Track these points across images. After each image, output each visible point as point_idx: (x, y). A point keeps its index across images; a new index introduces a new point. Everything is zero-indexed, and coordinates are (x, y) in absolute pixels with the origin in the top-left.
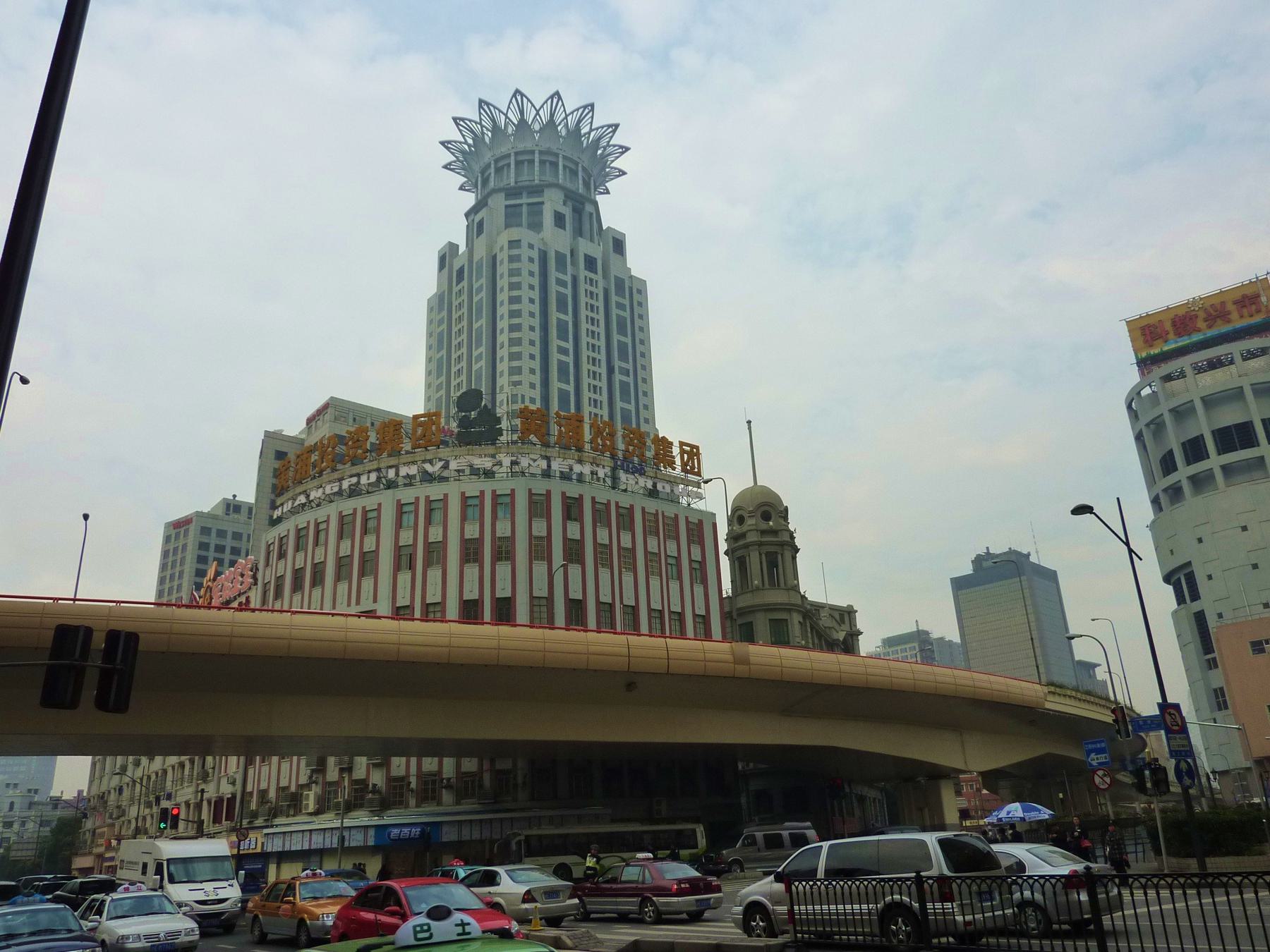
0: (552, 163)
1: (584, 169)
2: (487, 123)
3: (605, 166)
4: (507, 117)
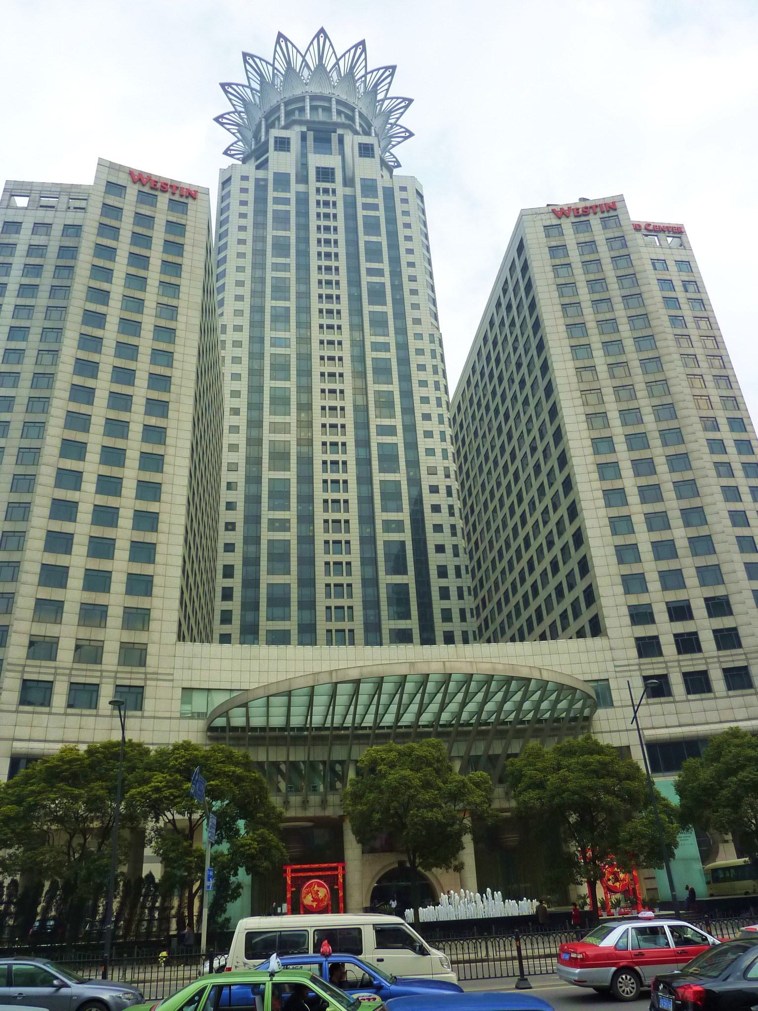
1: (361, 115)
2: (281, 66)
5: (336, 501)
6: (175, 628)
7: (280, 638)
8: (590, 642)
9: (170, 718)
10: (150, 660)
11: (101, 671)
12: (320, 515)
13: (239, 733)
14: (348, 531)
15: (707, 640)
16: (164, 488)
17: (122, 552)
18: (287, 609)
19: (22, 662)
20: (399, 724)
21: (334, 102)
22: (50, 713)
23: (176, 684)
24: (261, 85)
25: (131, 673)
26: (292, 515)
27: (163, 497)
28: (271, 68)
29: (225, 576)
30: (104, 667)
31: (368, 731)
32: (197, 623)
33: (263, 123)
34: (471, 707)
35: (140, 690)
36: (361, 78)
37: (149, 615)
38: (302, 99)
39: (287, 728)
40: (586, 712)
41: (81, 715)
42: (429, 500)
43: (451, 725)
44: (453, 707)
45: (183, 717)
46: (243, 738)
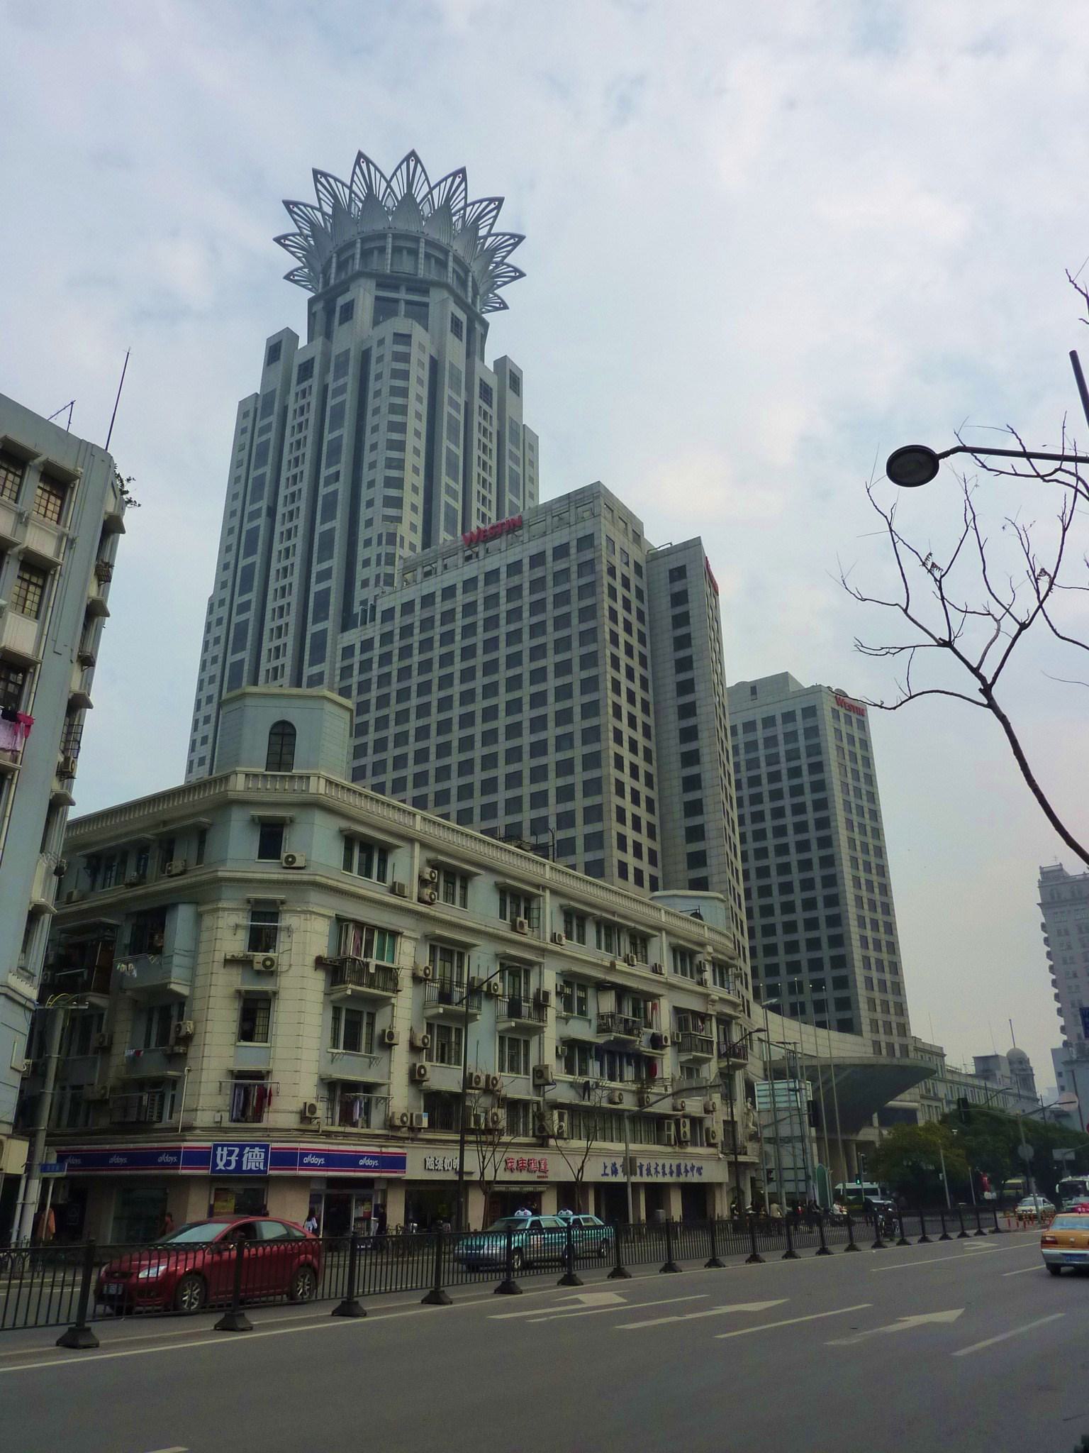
0: (438, 261)
2: (399, 188)
3: (493, 287)
4: (389, 186)
21: (422, 245)
24: (334, 208)
28: (347, 191)
33: (334, 260)
36: (459, 211)
38: (383, 236)
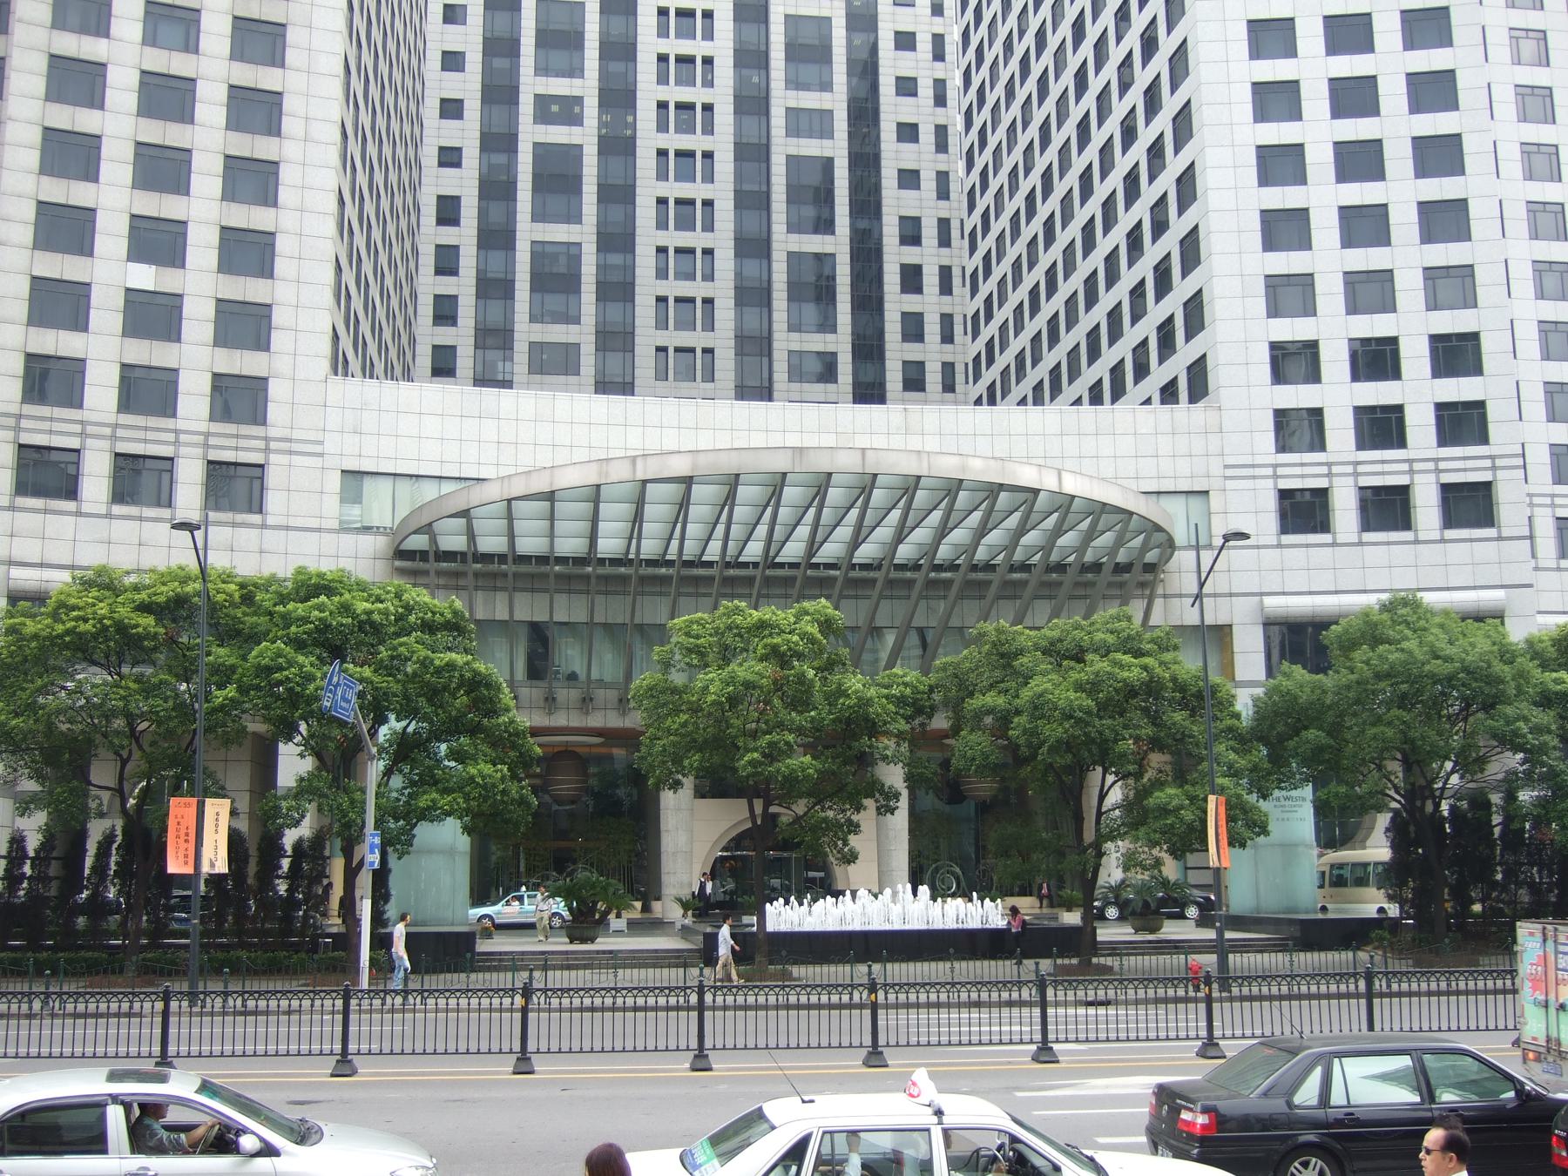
5: (685, 60)
6: (326, 347)
7: (554, 363)
8: (1182, 411)
9: (319, 530)
10: (273, 412)
11: (176, 432)
12: (649, 91)
13: (495, 567)
14: (709, 129)
15: (1421, 425)
16: (292, 36)
17: (207, 178)
18: (572, 298)
19: (14, 408)
20: (814, 560)
22: (79, 514)
23: (329, 462)
25: (237, 436)
26: (587, 87)
27: (291, 56)
29: (441, 221)
30: (181, 424)
31: (749, 572)
32: (376, 329)
34: (959, 536)
35: (258, 471)
37: (269, 317)
39: (589, 558)
40: (1151, 557)
41: (141, 519)
42: (891, 66)
43: (953, 567)
44: (921, 535)
45: (344, 528)
46: (464, 574)
